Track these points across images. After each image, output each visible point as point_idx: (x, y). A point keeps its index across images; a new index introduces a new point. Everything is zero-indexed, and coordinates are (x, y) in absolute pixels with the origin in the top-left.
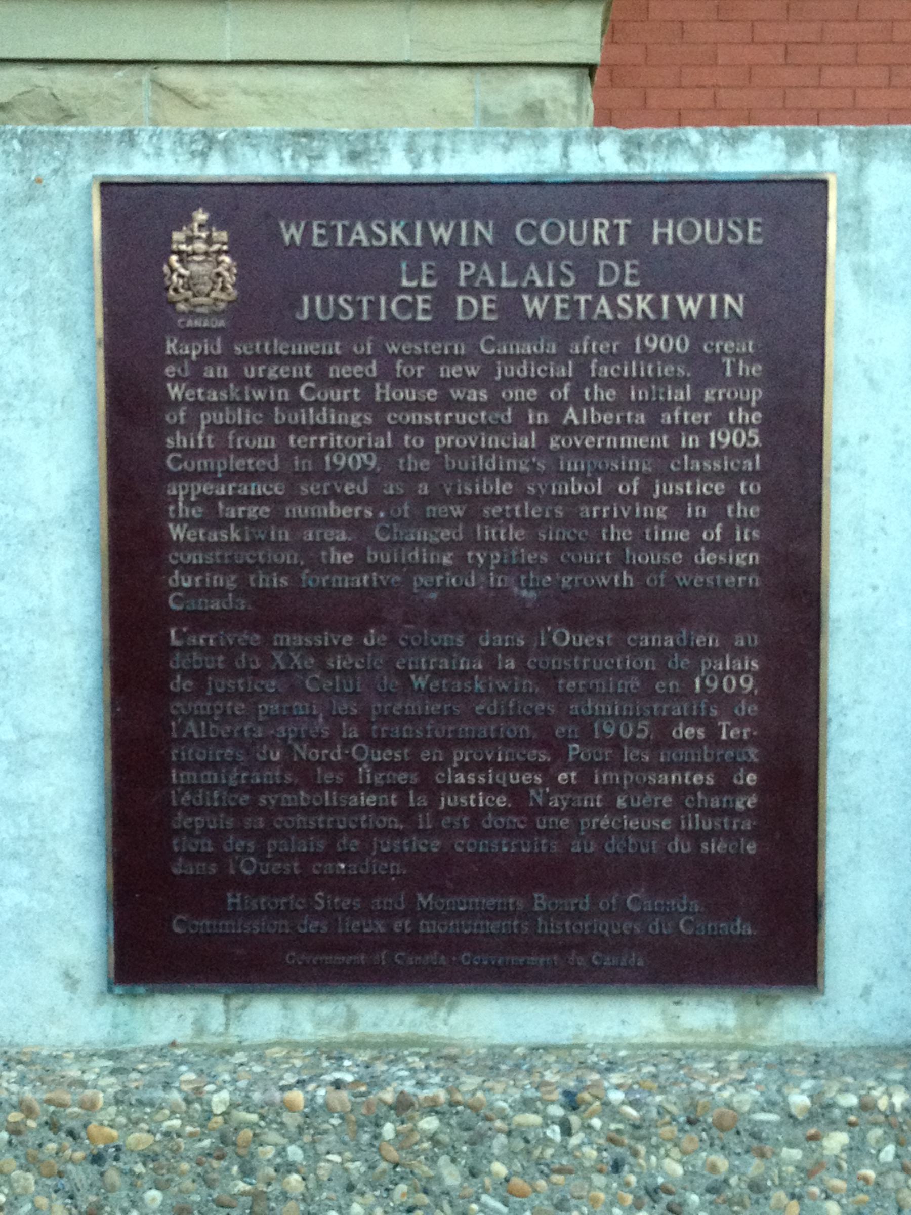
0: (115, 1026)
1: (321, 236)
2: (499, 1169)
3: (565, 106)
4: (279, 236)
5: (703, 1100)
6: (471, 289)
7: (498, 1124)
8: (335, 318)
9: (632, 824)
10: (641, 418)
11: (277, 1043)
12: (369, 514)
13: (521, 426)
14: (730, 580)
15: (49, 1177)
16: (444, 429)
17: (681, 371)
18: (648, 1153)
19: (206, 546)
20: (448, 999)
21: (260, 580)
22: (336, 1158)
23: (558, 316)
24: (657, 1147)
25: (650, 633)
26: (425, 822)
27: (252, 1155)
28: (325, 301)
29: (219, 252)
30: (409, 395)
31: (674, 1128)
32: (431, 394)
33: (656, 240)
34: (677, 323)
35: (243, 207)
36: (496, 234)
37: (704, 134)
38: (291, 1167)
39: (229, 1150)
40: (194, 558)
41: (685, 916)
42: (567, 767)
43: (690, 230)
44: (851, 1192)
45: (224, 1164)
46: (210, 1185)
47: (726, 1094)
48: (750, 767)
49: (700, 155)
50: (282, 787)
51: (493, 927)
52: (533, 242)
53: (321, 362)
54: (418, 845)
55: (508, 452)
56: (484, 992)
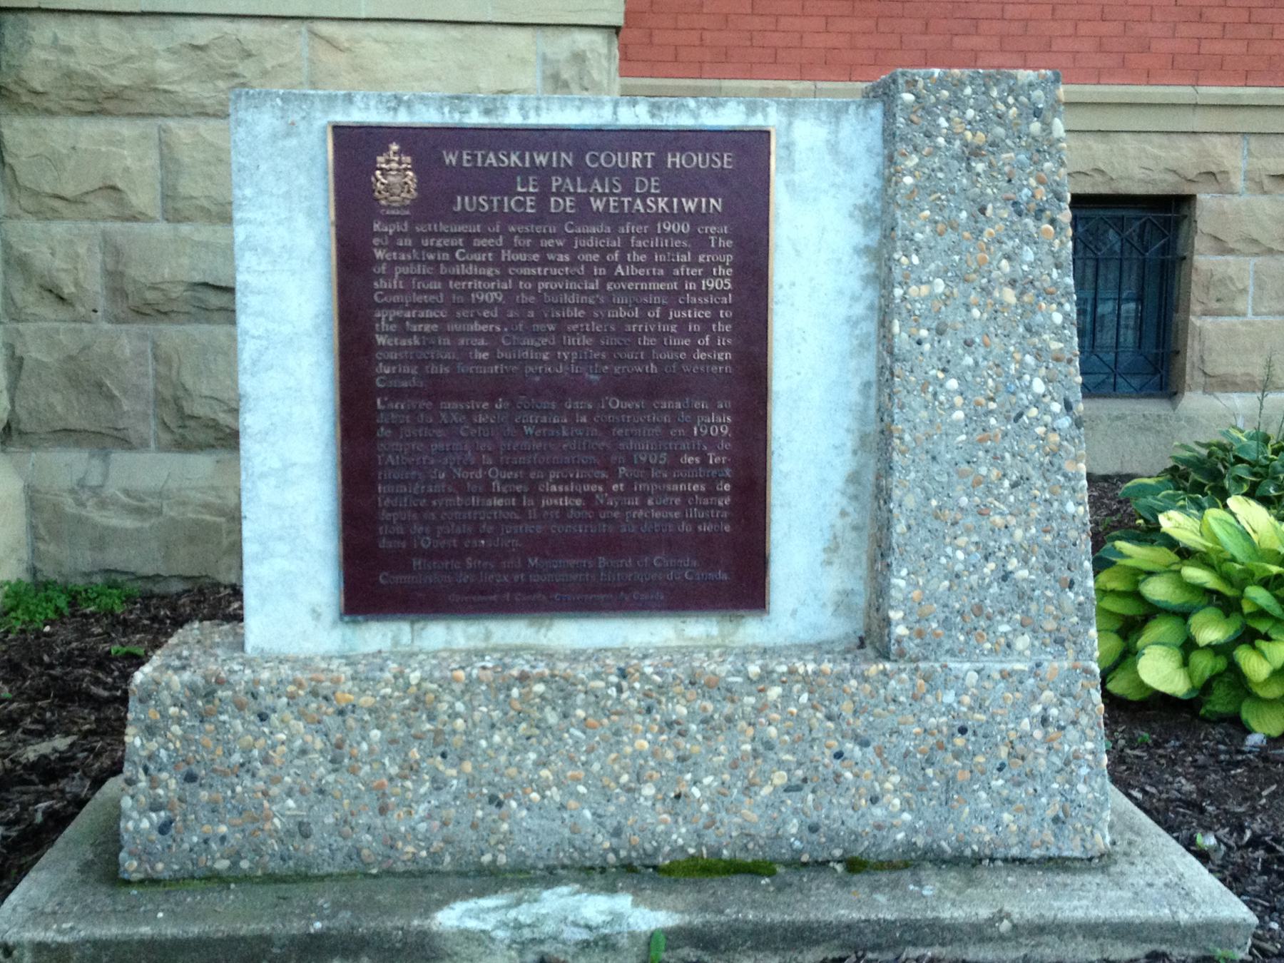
0: (344, 641)
1: (468, 161)
2: (581, 713)
3: (600, 55)
4: (441, 159)
5: (698, 671)
6: (558, 194)
7: (580, 687)
8: (477, 210)
9: (657, 515)
10: (661, 272)
11: (445, 650)
12: (498, 329)
13: (591, 277)
14: (714, 369)
15: (313, 723)
16: (543, 278)
17: (685, 244)
18: (667, 701)
19: (398, 348)
20: (547, 622)
21: (434, 369)
22: (484, 709)
23: (612, 210)
24: (673, 698)
25: (667, 400)
26: (532, 514)
27: (435, 708)
28: (471, 200)
29: (406, 169)
30: (522, 257)
31: (682, 687)
32: (536, 257)
33: (669, 166)
34: (682, 216)
35: (422, 143)
36: (575, 160)
37: (697, 102)
38: (457, 715)
39: (420, 706)
40: (393, 356)
41: (688, 569)
42: (618, 482)
43: (690, 160)
44: (783, 721)
45: (417, 714)
46: (409, 726)
47: (712, 667)
48: (726, 480)
49: (696, 115)
50: (447, 494)
51: (574, 577)
52: (596, 165)
53: (468, 237)
54: (529, 528)
55: (583, 292)
56: (570, 617)
